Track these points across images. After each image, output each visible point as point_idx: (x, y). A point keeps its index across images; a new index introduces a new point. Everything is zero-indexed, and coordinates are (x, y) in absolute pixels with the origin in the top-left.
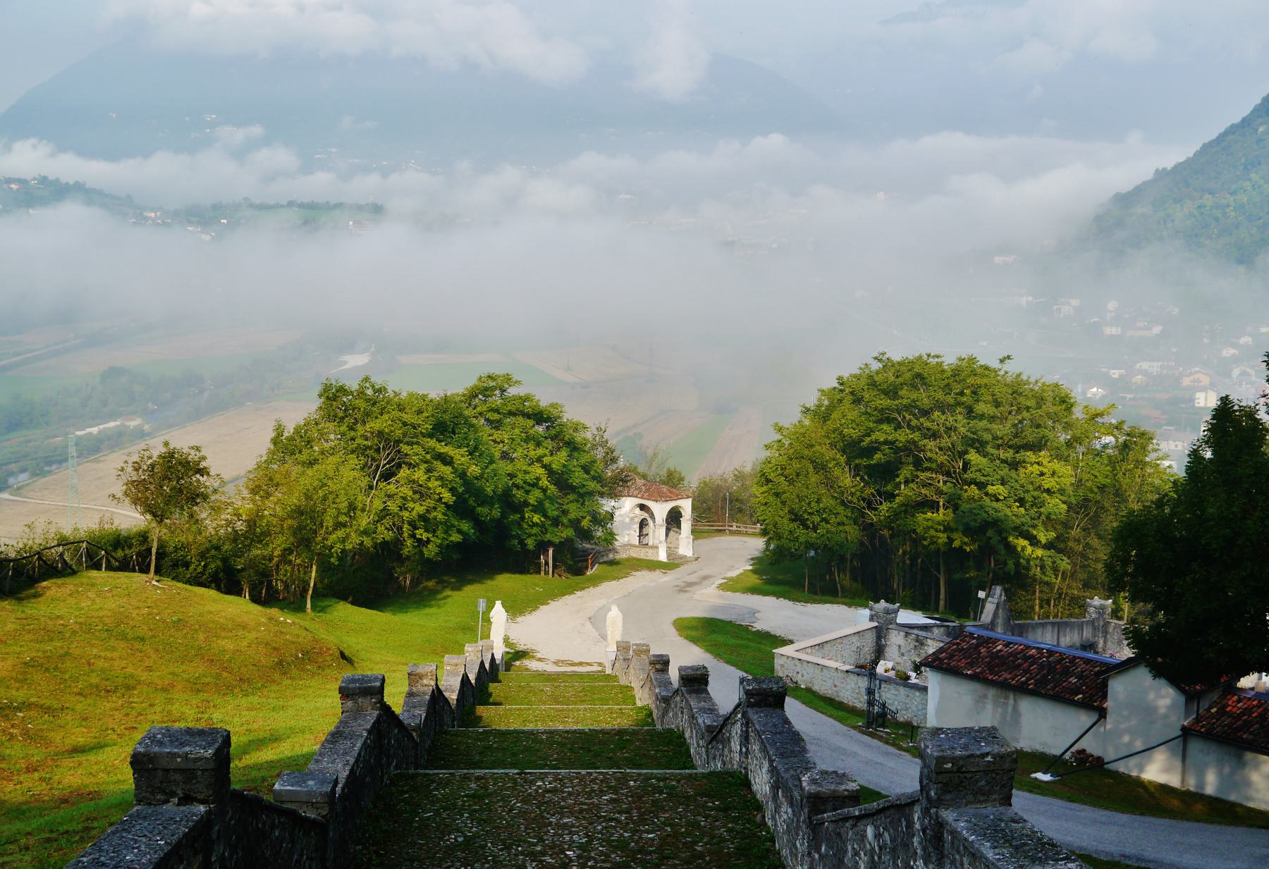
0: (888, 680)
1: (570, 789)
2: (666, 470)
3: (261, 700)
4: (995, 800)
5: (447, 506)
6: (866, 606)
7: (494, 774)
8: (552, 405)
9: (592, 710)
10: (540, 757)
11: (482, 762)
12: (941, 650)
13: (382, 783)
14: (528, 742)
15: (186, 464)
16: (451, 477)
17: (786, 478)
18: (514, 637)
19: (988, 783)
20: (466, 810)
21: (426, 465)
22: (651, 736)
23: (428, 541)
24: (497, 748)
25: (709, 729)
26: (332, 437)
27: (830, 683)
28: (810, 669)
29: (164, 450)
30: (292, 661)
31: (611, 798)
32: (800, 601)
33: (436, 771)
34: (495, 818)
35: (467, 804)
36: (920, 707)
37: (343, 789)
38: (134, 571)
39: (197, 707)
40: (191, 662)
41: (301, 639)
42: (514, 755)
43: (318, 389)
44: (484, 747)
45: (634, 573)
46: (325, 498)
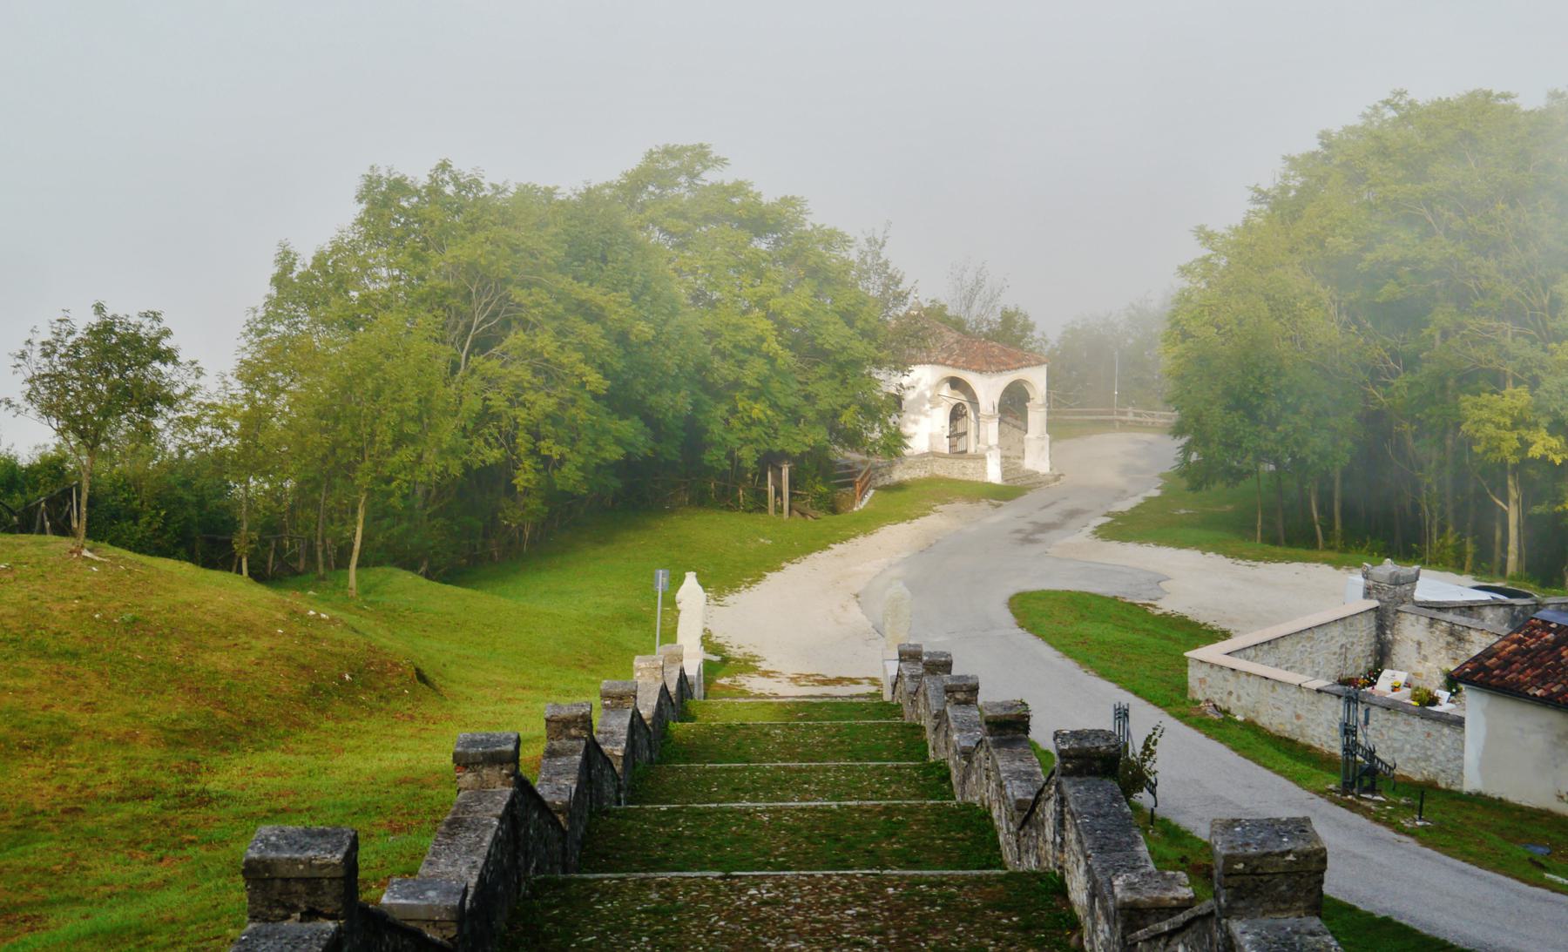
0: (1391, 707)
1: (798, 900)
2: (998, 310)
3: (284, 757)
4: (1299, 908)
5: (596, 397)
6: (1358, 566)
7: (685, 878)
8: (787, 201)
9: (850, 770)
10: (758, 851)
11: (667, 859)
12: (1489, 653)
13: (519, 893)
14: (739, 826)
15: (133, 342)
16: (603, 344)
17: (1219, 328)
18: (720, 635)
19: (1290, 887)
20: (644, 931)
21: (556, 324)
22: (938, 815)
23: (562, 461)
24: (690, 837)
25: (1020, 805)
26: (384, 272)
27: (1287, 712)
28: (1252, 687)
29: (95, 320)
30: (335, 688)
31: (858, 912)
32: (1244, 558)
33: (599, 875)
34: (688, 943)
35: (645, 923)
36: (1451, 756)
37: (471, 902)
38: (42, 531)
39: (180, 771)
40: (162, 693)
41: (347, 649)
42: (717, 847)
43: (355, 184)
44: (669, 836)
45: (940, 507)
46: (378, 393)
